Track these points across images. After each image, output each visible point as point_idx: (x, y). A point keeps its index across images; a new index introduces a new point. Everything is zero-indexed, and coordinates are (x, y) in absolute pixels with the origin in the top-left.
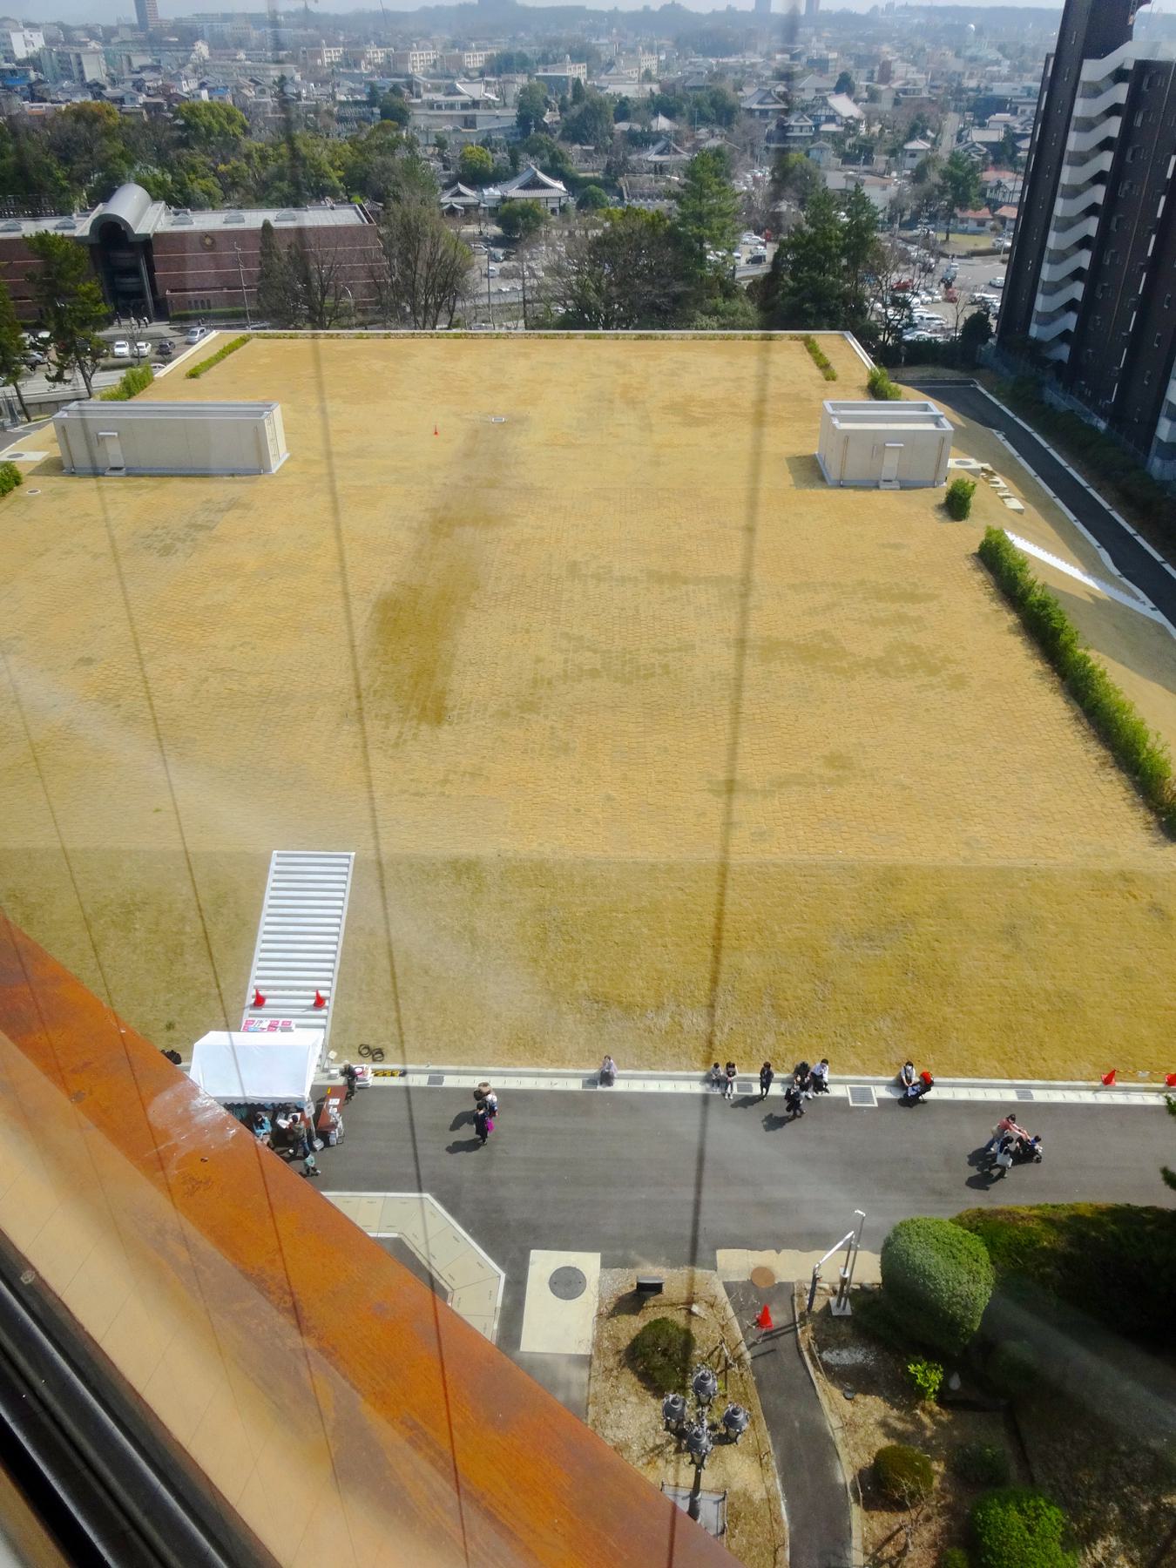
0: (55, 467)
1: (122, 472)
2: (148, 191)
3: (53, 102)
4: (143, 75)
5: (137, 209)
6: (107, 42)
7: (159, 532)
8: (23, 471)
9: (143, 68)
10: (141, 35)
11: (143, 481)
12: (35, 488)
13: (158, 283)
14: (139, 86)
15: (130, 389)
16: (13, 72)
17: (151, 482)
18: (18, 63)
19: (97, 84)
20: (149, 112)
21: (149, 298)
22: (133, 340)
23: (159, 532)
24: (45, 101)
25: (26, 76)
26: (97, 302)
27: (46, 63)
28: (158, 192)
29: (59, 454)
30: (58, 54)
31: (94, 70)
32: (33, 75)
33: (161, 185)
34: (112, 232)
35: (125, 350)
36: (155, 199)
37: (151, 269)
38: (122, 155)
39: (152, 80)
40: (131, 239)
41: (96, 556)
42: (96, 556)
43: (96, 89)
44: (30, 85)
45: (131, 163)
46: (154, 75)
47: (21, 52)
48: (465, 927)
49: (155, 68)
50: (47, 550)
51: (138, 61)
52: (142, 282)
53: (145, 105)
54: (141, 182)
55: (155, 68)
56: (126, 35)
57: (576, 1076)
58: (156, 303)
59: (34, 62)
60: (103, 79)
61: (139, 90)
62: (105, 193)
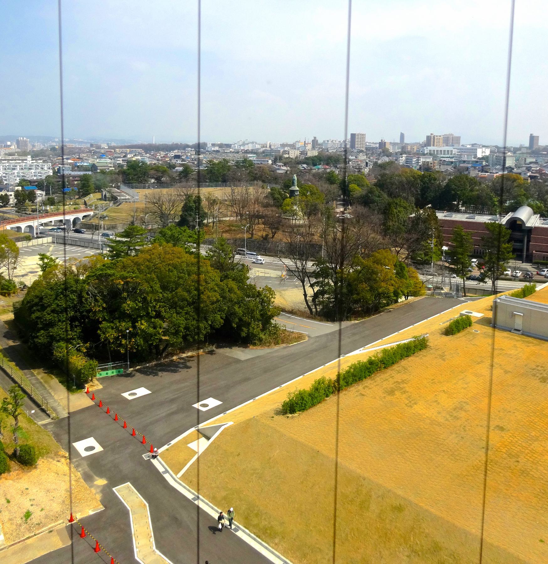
0: (485, 321)
1: (520, 333)
2: (533, 210)
3: (491, 173)
4: (532, 165)
5: (527, 216)
6: (514, 153)
7: (539, 368)
8: (473, 320)
9: (531, 163)
10: (529, 151)
11: (530, 339)
12: (476, 329)
13: (530, 247)
14: (529, 169)
15: (525, 293)
16: (477, 162)
17: (535, 341)
18: (479, 158)
19: (510, 167)
20: (531, 179)
21: (525, 253)
22: (514, 269)
23: (539, 368)
24: (487, 172)
25: (482, 164)
26: (508, 252)
27: (490, 159)
28: (536, 211)
29: (491, 317)
30: (496, 156)
31: (510, 163)
32: (484, 163)
33: (539, 208)
34: (515, 224)
35: (509, 273)
36: (535, 213)
37: (529, 241)
38: (524, 195)
39: (535, 167)
40: (523, 228)
41: (506, 372)
42: (506, 372)
43: (511, 169)
44: (482, 167)
45: (528, 198)
46: (535, 166)
47: (479, 155)
48: (232, 465)
49: (536, 163)
50: (482, 362)
51: (529, 160)
52: (523, 246)
53: (530, 176)
54: (529, 205)
55: (536, 163)
56: (524, 151)
57: (193, 494)
58: (527, 256)
59: (485, 158)
60: (513, 165)
61: (529, 170)
62: (514, 208)
